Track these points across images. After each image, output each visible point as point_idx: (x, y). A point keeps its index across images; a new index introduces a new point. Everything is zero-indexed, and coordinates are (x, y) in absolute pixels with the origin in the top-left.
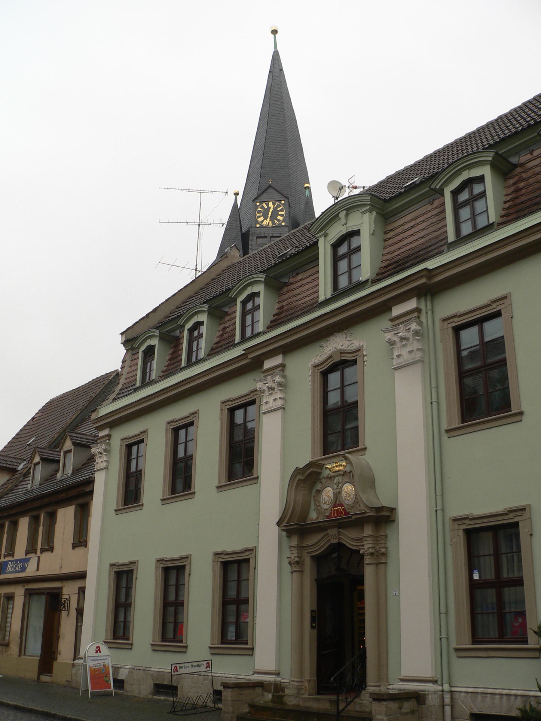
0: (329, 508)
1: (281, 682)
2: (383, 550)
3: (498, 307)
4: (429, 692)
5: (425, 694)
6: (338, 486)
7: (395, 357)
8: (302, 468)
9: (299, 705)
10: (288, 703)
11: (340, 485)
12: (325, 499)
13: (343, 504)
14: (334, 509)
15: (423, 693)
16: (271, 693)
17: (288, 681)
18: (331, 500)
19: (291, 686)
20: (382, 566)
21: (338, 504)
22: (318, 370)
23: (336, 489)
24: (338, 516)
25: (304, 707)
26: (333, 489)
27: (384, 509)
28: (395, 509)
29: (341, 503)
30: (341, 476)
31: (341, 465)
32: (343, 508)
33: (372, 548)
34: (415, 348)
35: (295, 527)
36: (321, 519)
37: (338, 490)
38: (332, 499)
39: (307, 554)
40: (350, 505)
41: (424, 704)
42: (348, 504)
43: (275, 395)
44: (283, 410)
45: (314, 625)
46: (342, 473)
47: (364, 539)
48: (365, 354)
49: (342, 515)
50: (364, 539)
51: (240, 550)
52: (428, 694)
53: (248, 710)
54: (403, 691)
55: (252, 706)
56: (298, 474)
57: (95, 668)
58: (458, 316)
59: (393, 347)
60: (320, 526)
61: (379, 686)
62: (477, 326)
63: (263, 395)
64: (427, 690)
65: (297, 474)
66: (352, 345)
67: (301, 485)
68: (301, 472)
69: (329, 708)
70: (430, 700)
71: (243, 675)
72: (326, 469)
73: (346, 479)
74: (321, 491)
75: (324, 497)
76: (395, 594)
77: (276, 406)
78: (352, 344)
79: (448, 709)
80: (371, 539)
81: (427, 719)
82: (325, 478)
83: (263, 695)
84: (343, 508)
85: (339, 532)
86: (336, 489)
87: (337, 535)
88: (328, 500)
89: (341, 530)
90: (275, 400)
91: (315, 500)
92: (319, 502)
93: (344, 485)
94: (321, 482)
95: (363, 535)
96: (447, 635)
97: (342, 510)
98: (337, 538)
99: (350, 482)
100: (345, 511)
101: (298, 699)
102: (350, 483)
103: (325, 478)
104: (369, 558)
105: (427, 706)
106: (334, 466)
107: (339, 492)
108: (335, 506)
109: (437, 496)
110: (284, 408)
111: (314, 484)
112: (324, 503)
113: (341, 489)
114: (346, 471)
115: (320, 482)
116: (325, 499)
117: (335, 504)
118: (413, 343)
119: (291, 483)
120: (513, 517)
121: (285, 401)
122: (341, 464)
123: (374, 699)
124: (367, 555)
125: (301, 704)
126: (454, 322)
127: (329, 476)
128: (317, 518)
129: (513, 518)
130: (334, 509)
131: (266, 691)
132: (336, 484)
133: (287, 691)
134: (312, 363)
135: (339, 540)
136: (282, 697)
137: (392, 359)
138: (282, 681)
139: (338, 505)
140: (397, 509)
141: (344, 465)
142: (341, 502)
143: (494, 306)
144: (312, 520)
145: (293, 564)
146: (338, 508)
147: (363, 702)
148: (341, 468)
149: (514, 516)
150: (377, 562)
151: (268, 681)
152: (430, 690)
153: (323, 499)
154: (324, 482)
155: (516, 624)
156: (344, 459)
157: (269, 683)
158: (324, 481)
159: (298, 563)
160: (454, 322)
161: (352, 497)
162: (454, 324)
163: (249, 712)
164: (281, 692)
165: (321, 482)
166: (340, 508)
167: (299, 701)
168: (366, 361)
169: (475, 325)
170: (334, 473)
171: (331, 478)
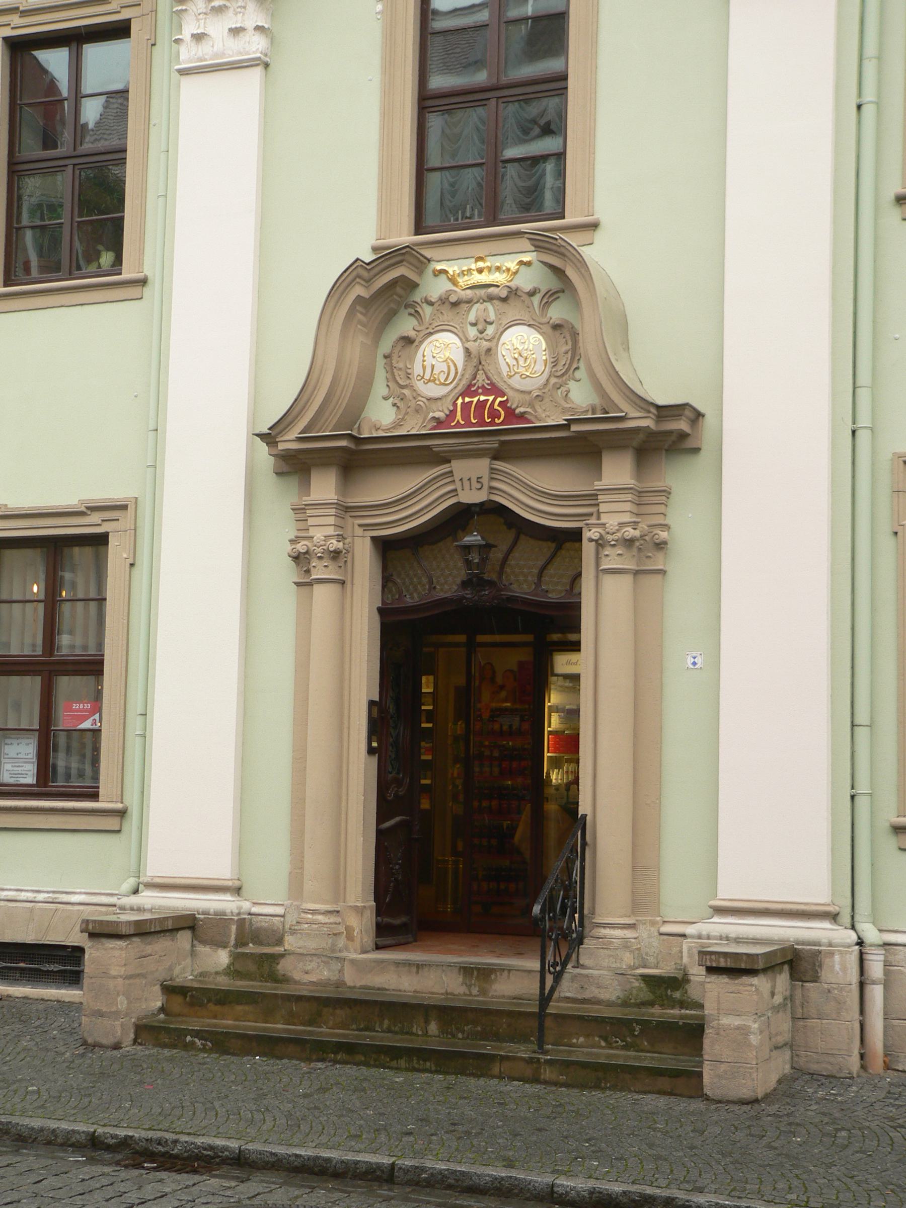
0: (445, 396)
1: (250, 914)
2: (664, 535)
3: (123, 10)
4: (830, 945)
5: (820, 952)
6: (481, 332)
7: (186, 35)
8: (368, 264)
9: (340, 984)
10: (297, 976)
11: (490, 330)
12: (433, 367)
14: (467, 400)
15: (810, 950)
16: (225, 947)
17: (280, 910)
18: (456, 373)
19: (306, 926)
20: (649, 581)
21: (483, 387)
23: (475, 341)
24: (482, 423)
25: (362, 987)
26: (464, 339)
27: (687, 412)
28: (703, 416)
30: (496, 302)
31: (498, 269)
32: (499, 399)
33: (635, 525)
34: (250, 24)
35: (343, 443)
36: (413, 426)
37: (486, 345)
39: (359, 531)
40: (530, 392)
41: (816, 979)
42: (518, 387)
43: (236, 14)
44: (263, 70)
45: (375, 744)
46: (504, 293)
49: (497, 421)
51: (74, 506)
52: (832, 954)
53: (159, 1004)
54: (780, 944)
55: (170, 990)
56: (358, 280)
58: (22, 12)
59: (184, 8)
60: (428, 447)
61: (632, 926)
62: (67, 49)
63: (186, 10)
64: (825, 941)
65: (355, 279)
67: (359, 316)
68: (365, 274)
69: (462, 990)
70: (837, 967)
71: (80, 893)
72: (436, 275)
73: (513, 311)
74: (416, 343)
75: (429, 361)
76: (694, 664)
77: (241, 54)
79: (876, 994)
80: (629, 497)
81: (824, 1021)
82: (431, 304)
83: (193, 953)
84: (499, 399)
85: (492, 470)
86: (475, 341)
87: (485, 481)
88: (446, 370)
90: (236, 31)
91: (390, 369)
92: (408, 376)
94: (417, 315)
95: (598, 485)
96: (872, 785)
97: (496, 407)
98: (486, 487)
99: (532, 322)
100: (510, 408)
101: (336, 966)
102: (529, 325)
103: (431, 304)
104: (619, 554)
105: (826, 986)
106: (469, 270)
107: (489, 350)
108: (468, 391)
109: (858, 391)
110: (266, 65)
111: (390, 316)
112: (429, 381)
113: (495, 340)
114: (517, 289)
115: (410, 314)
116: (433, 367)
117: (470, 386)
118: (244, 7)
119: (331, 304)
120: (100, 522)
121: (272, 43)
122: (498, 264)
123: (711, 970)
124: (614, 545)
125: (351, 978)
127: (453, 299)
128: (397, 424)
130: (467, 400)
131: (204, 942)
132: (474, 325)
133: (290, 943)
135: (488, 497)
136: (274, 958)
137: (177, 41)
138: (255, 910)
140: (709, 421)
141: (508, 270)
142: (496, 379)
144: (377, 429)
145: (320, 558)
146: (482, 398)
147: (595, 972)
148: (499, 278)
149: (103, 521)
150: (637, 568)
151: (212, 911)
152: (713, 934)
153: (424, 368)
154: (428, 317)
156: (533, 248)
157: (220, 920)
158: (427, 311)
159: (336, 555)
161: (540, 367)
162: (8, 32)
163: (162, 1009)
164: (251, 945)
165: (417, 315)
166: (491, 398)
167: (341, 971)
169: (63, 46)
170: (469, 292)
171: (455, 304)
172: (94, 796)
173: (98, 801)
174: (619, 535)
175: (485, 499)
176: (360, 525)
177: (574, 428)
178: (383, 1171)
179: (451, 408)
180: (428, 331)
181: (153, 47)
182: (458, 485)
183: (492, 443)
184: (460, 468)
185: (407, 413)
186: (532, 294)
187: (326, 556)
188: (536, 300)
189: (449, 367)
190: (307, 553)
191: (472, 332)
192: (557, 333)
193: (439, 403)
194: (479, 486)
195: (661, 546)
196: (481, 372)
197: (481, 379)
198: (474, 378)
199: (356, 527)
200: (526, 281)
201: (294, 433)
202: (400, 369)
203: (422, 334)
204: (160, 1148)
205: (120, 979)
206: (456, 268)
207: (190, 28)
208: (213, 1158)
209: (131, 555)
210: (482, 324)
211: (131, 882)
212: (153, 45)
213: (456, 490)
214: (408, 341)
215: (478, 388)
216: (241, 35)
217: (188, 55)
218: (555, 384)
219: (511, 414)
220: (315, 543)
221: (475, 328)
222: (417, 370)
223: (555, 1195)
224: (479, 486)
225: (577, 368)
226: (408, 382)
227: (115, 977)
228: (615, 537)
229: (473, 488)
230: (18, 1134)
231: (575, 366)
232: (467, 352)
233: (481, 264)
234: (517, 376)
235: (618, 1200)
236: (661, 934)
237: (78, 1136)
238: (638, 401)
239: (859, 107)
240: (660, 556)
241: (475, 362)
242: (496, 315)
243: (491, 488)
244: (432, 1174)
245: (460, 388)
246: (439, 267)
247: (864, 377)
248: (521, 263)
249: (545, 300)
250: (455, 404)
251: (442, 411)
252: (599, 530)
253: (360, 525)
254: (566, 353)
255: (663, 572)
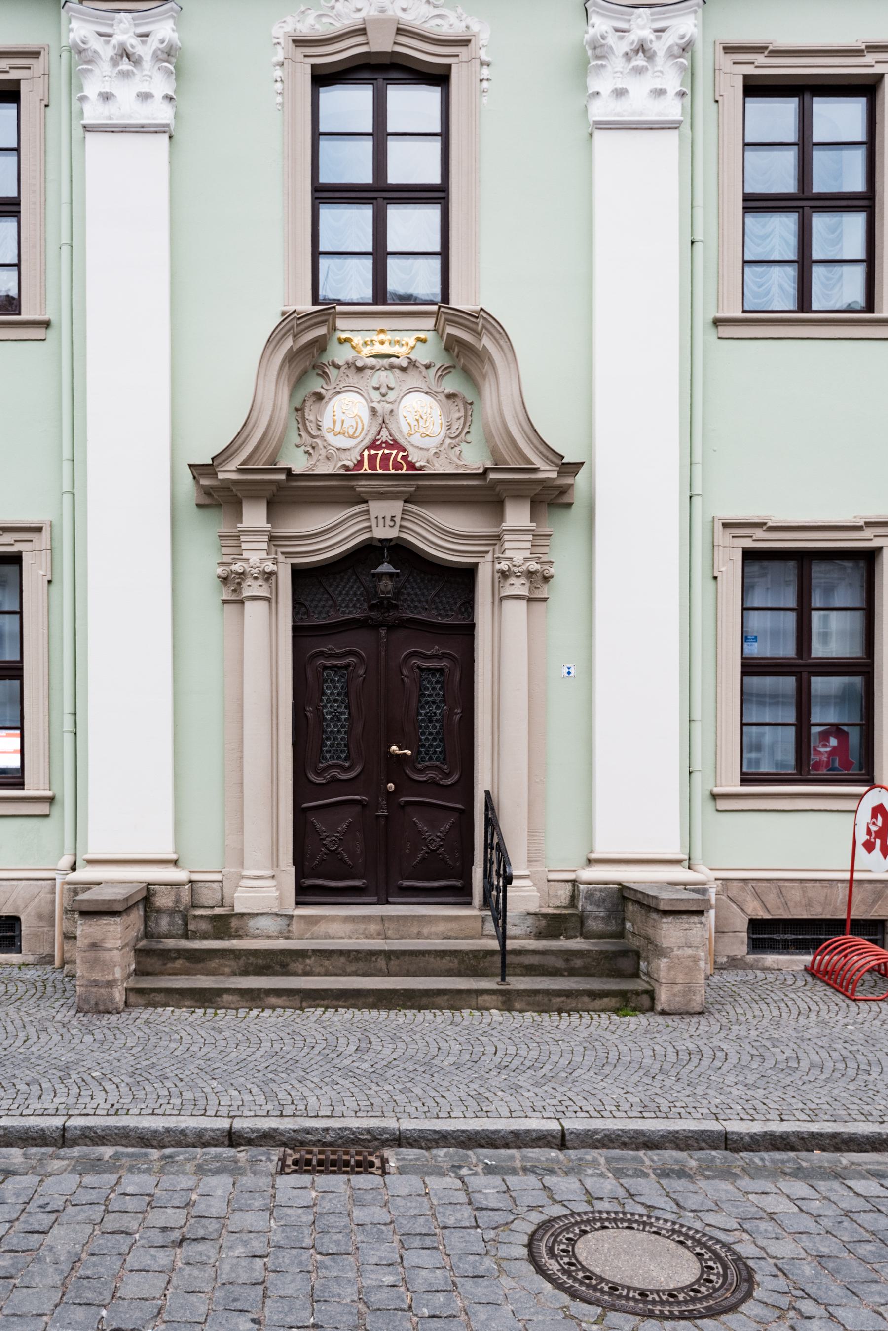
3: (12, 71)
11: (391, 396)
12: (343, 422)
13: (402, 441)
14: (373, 452)
17: (218, 877)
18: (363, 429)
20: (538, 607)
21: (386, 442)
22: (305, 56)
29: (394, 440)
30: (397, 371)
37: (388, 407)
38: (365, 427)
39: (281, 558)
40: (428, 450)
46: (405, 364)
47: (506, 537)
48: (485, 57)
50: (506, 537)
57: (73, 1122)
58: (772, 52)
59: (89, 67)
66: (438, 21)
73: (412, 380)
74: (324, 401)
76: (569, 673)
78: (439, 16)
89: (411, 507)
93: (403, 397)
97: (399, 459)
98: (398, 525)
99: (429, 391)
102: (427, 393)
103: (338, 367)
107: (392, 411)
108: (373, 445)
113: (397, 403)
115: (318, 375)
116: (343, 422)
117: (376, 440)
119: (269, 351)
120: (12, 542)
126: (753, 63)
129: (12, 545)
130: (373, 452)
134: (289, 28)
139: (384, 445)
143: (870, 58)
145: (256, 578)
146: (386, 451)
148: (401, 351)
149: (16, 541)
153: (334, 422)
155: (822, 750)
160: (753, 63)
166: (394, 452)
168: (488, 80)
170: (372, 359)
171: (360, 370)
172: (21, 785)
173: (23, 789)
174: (524, 568)
175: (396, 535)
176: (283, 553)
177: (492, 476)
178: (554, 1137)
179: (359, 458)
180: (336, 390)
181: (47, 109)
182: (374, 521)
183: (409, 487)
184: (377, 508)
185: (318, 460)
186: (428, 367)
187: (261, 577)
188: (432, 371)
189: (357, 423)
190: (243, 573)
191: (376, 396)
192: (450, 402)
193: (347, 453)
194: (392, 524)
195: (546, 579)
196: (384, 429)
197: (384, 436)
198: (379, 434)
199: (279, 554)
200: (423, 355)
201: (234, 464)
202: (311, 421)
203: (331, 392)
204: (310, 1137)
205: (116, 952)
206: (359, 338)
207: (92, 89)
208: (369, 1141)
209: (49, 573)
210: (383, 391)
211: (65, 861)
212: (46, 106)
213: (370, 527)
214: (319, 397)
215: (382, 443)
216: (149, 100)
217: (94, 113)
218: (450, 444)
219: (411, 466)
220: (251, 564)
221: (377, 392)
222: (326, 423)
223: (729, 1142)
224: (392, 524)
225: (468, 432)
226: (319, 433)
227: (110, 950)
228: (520, 569)
229: (387, 525)
230: (139, 1138)
231: (466, 430)
232: (374, 411)
233: (382, 337)
234: (418, 435)
235: (788, 1141)
236: (548, 881)
237: (212, 1134)
238: (551, 456)
239: (692, 243)
240: (546, 587)
241: (380, 420)
242: (396, 382)
243: (401, 526)
244: (606, 1135)
245: (367, 442)
246: (344, 335)
247: (697, 458)
248: (419, 340)
249: (439, 373)
250: (362, 456)
251: (351, 460)
252: (507, 563)
253: (283, 553)
254: (459, 419)
255: (545, 600)
